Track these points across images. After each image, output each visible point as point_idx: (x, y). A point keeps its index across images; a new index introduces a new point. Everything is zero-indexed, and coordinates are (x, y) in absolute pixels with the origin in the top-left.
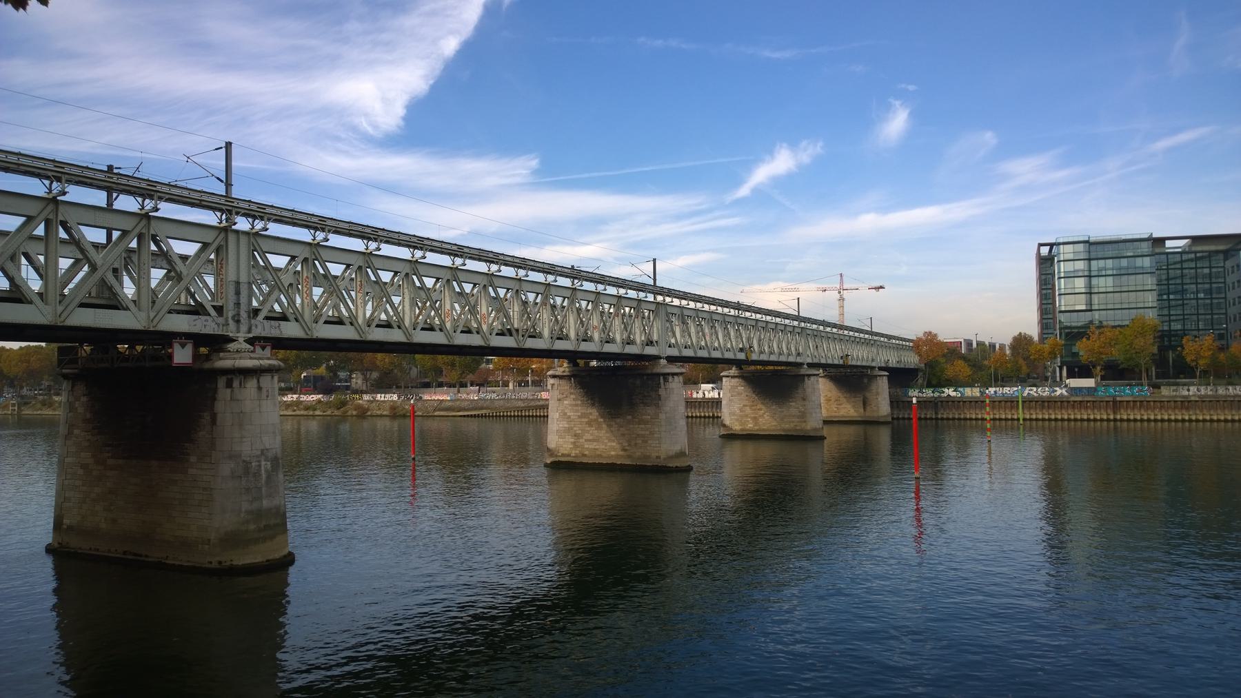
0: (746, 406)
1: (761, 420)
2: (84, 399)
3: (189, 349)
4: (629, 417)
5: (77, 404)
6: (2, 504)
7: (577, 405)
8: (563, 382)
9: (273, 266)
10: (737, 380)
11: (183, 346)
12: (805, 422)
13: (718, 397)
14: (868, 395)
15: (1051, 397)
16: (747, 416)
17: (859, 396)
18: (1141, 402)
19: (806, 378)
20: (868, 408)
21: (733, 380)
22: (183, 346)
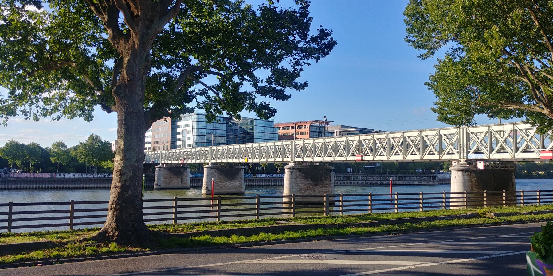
0: (218, 181)
1: (224, 187)
2: (475, 178)
3: (482, 163)
4: (321, 185)
5: (473, 180)
6: (545, 196)
7: (302, 181)
8: (296, 171)
9: (200, 84)
10: (214, 170)
11: (480, 163)
12: (241, 188)
13: (73, 177)
14: (183, 176)
15: (20, 178)
16: (218, 186)
17: (179, 177)
18: (195, 180)
19: (242, 169)
20: (183, 183)
21: (212, 170)
22: (480, 163)
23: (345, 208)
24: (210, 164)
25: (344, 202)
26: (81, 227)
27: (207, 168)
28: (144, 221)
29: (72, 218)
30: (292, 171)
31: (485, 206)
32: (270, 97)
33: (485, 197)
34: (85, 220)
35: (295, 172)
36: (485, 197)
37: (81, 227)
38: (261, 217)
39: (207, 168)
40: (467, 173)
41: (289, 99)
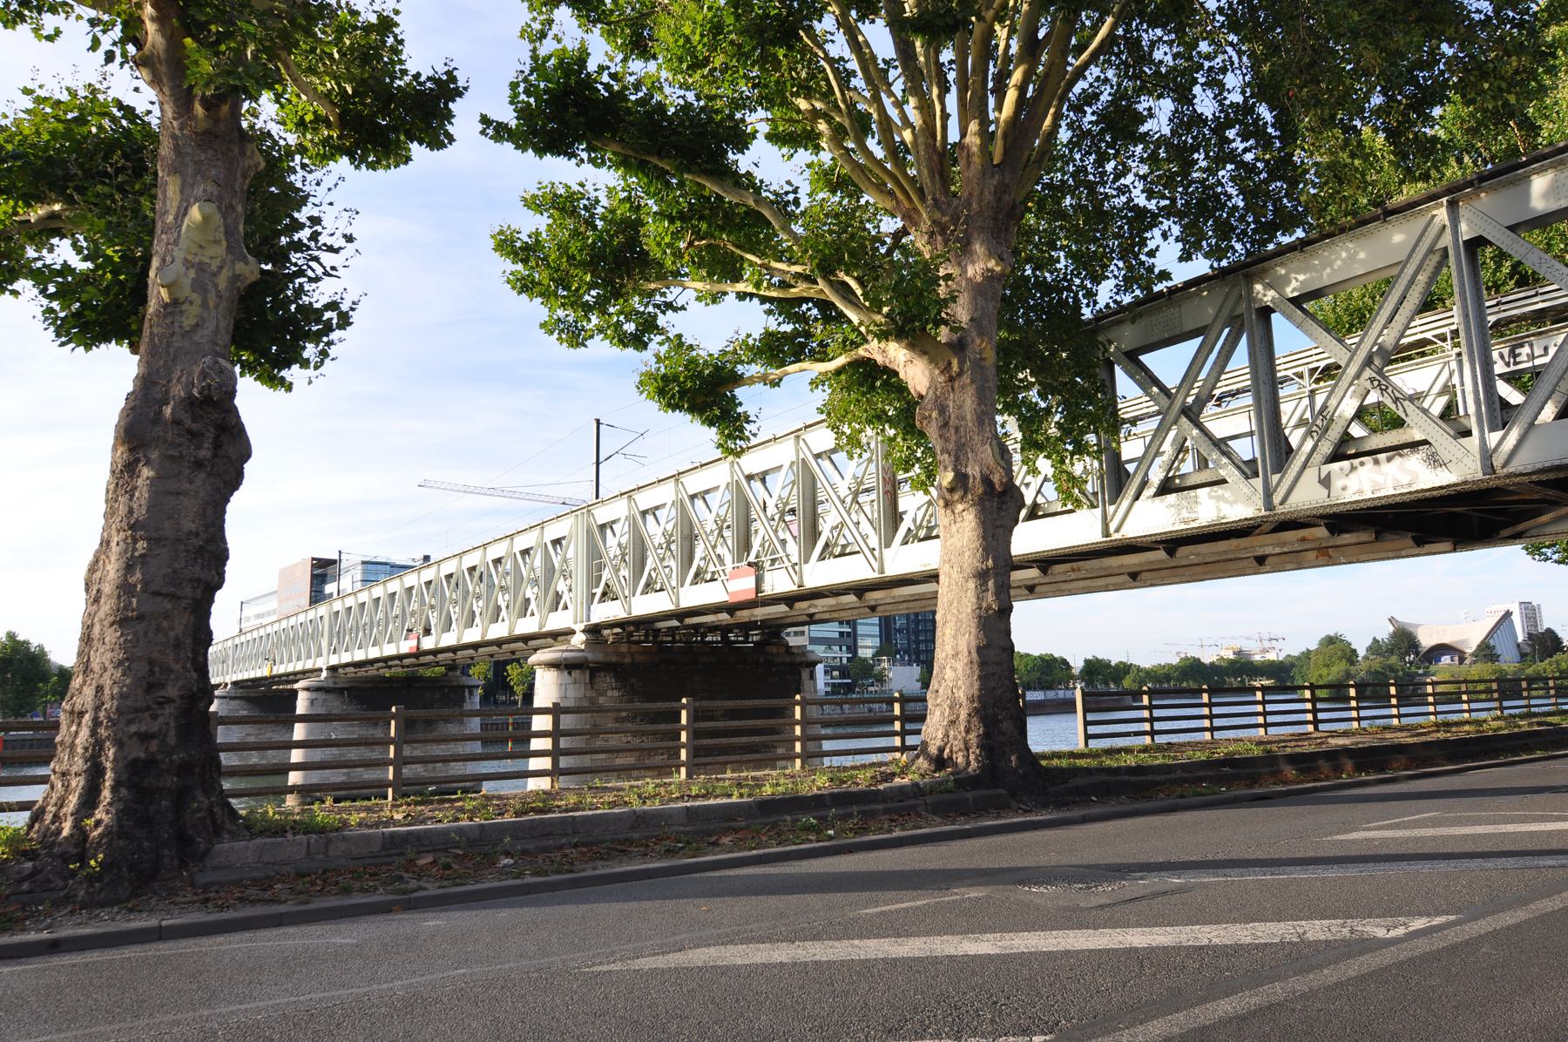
8: (331, 697)
10: (238, 702)
23: (1270, 719)
24: (579, 640)
25: (406, 763)
26: (1174, 738)
27: (307, 689)
28: (224, 796)
29: (1315, 711)
30: (315, 695)
31: (798, 762)
32: (522, 36)
33: (1393, 696)
34: (505, 767)
35: (325, 701)
36: (1393, 696)
37: (1174, 738)
38: (1160, 739)
39: (307, 689)
40: (576, 673)
41: (467, 95)
